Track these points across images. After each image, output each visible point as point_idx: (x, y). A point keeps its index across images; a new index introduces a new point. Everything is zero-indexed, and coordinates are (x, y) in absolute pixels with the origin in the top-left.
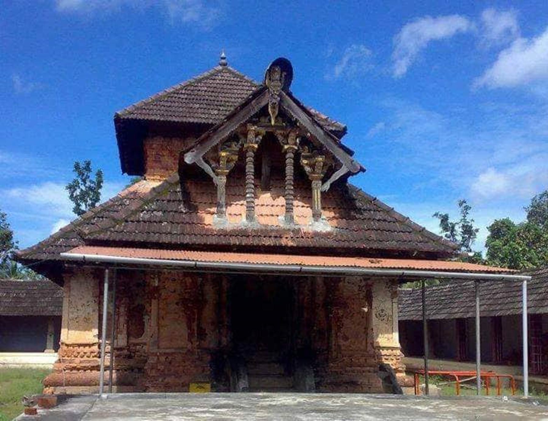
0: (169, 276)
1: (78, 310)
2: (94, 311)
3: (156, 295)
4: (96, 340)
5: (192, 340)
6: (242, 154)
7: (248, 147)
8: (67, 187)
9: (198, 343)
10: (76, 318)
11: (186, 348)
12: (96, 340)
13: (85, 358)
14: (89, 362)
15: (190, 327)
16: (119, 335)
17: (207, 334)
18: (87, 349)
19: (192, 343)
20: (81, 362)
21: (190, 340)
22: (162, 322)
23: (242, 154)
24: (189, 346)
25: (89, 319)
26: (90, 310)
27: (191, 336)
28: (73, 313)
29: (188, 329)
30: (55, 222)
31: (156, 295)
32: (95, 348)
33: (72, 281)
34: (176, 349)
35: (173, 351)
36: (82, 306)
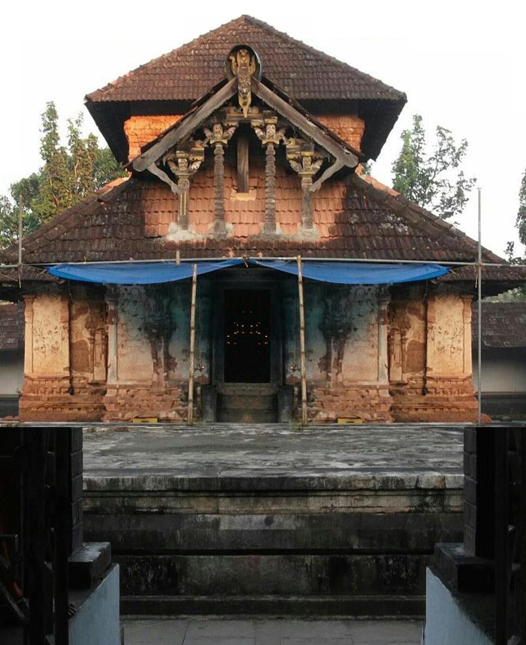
0: (129, 298)
1: (44, 338)
2: (63, 339)
3: (113, 320)
4: (67, 373)
5: (159, 371)
6: (209, 152)
7: (267, 143)
8: (393, 169)
9: (165, 374)
10: (42, 348)
11: (152, 380)
12: (67, 373)
13: (55, 394)
14: (60, 399)
15: (155, 356)
16: (95, 368)
17: (176, 364)
18: (56, 384)
19: (158, 374)
20: (49, 399)
21: (155, 371)
22: (121, 350)
23: (209, 152)
24: (155, 377)
25: (58, 349)
26: (58, 338)
27: (157, 365)
28: (37, 341)
29: (153, 358)
30: (176, 221)
31: (113, 320)
32: (67, 382)
33: (34, 303)
34: (139, 381)
35: (136, 383)
36: (49, 334)
